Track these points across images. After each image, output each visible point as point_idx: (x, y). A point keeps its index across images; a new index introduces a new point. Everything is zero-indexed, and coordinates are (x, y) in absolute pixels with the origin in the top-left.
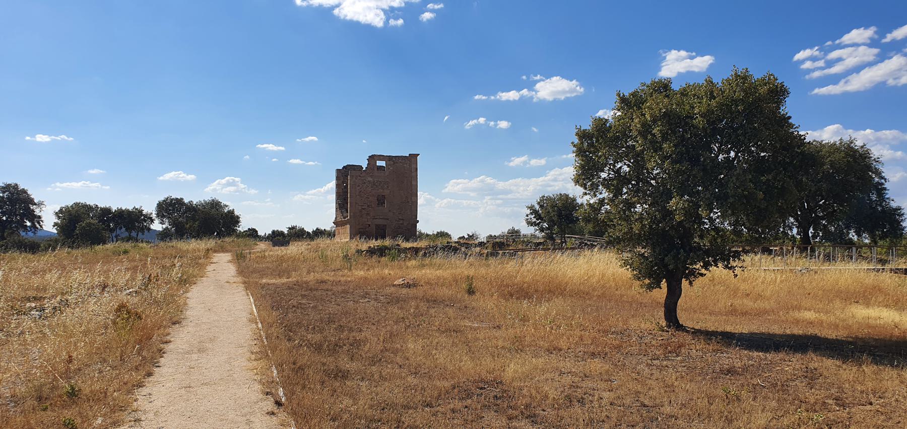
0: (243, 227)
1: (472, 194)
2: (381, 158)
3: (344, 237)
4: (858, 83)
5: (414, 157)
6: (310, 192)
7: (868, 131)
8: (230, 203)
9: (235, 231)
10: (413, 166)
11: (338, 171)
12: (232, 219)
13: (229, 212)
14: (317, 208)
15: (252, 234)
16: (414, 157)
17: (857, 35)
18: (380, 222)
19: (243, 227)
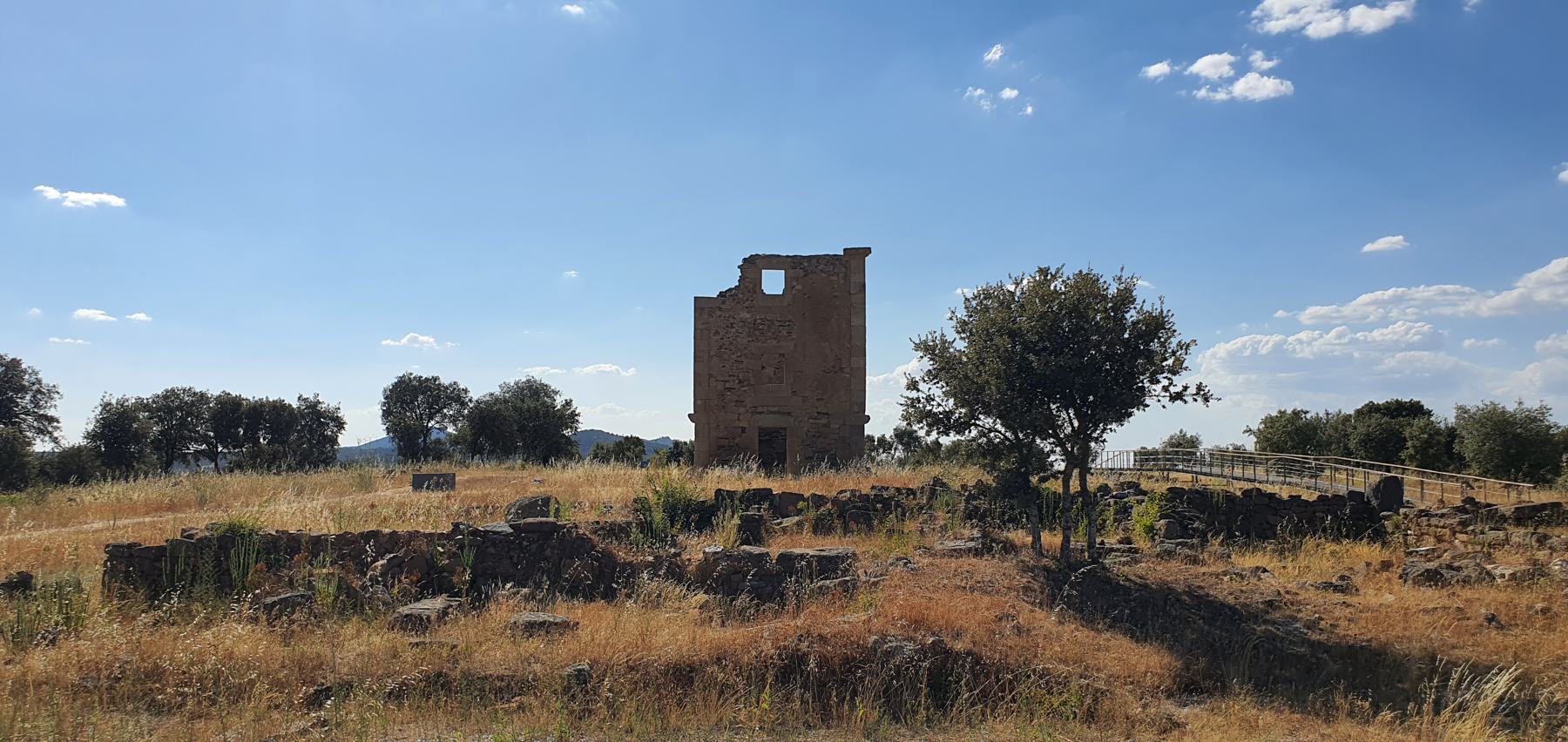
2: (773, 261)
5: (857, 256)
10: (854, 279)
16: (857, 256)
18: (768, 421)
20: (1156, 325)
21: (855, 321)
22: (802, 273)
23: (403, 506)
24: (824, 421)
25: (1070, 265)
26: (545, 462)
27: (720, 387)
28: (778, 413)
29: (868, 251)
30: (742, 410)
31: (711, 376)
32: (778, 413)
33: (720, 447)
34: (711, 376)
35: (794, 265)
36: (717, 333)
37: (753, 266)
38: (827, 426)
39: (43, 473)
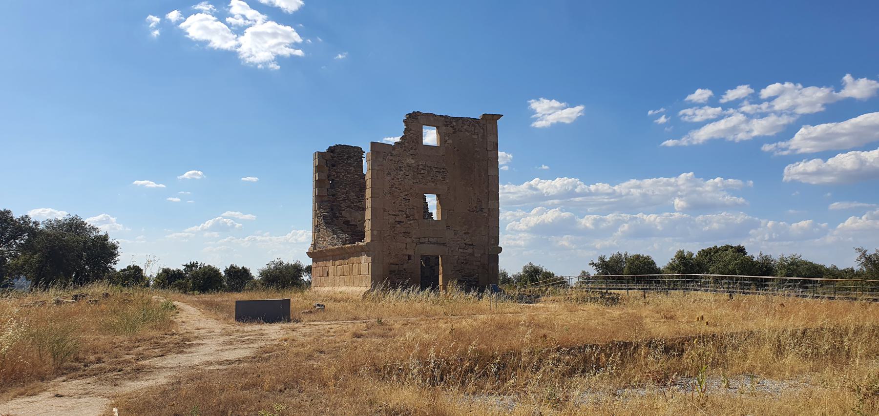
0: (121, 264)
1: (556, 201)
2: (432, 120)
3: (349, 284)
4: (703, 135)
5: (491, 120)
6: (187, 230)
7: (718, 179)
8: (101, 222)
9: (106, 269)
10: (490, 139)
11: (320, 155)
12: (104, 250)
13: (99, 238)
14: (278, 231)
15: (134, 275)
16: (491, 120)
17: (701, 95)
18: (429, 250)
19: (121, 264)
20: (114, 247)
21: (491, 172)
22: (451, 130)
23: (594, 319)
24: (470, 251)
25: (73, 215)
26: (185, 292)
27: (392, 220)
28: (437, 243)
29: (496, 117)
30: (408, 240)
31: (384, 210)
32: (437, 243)
33: (391, 272)
34: (384, 210)
35: (447, 125)
36: (389, 174)
37: (415, 122)
38: (472, 254)
39: (110, 278)
